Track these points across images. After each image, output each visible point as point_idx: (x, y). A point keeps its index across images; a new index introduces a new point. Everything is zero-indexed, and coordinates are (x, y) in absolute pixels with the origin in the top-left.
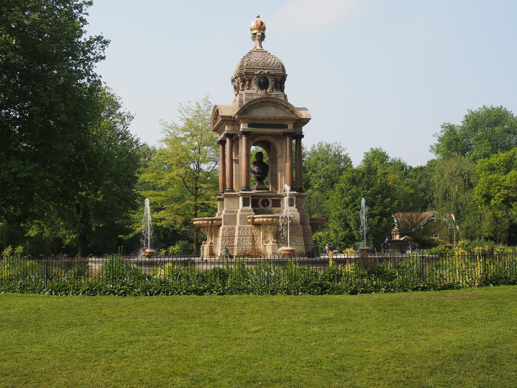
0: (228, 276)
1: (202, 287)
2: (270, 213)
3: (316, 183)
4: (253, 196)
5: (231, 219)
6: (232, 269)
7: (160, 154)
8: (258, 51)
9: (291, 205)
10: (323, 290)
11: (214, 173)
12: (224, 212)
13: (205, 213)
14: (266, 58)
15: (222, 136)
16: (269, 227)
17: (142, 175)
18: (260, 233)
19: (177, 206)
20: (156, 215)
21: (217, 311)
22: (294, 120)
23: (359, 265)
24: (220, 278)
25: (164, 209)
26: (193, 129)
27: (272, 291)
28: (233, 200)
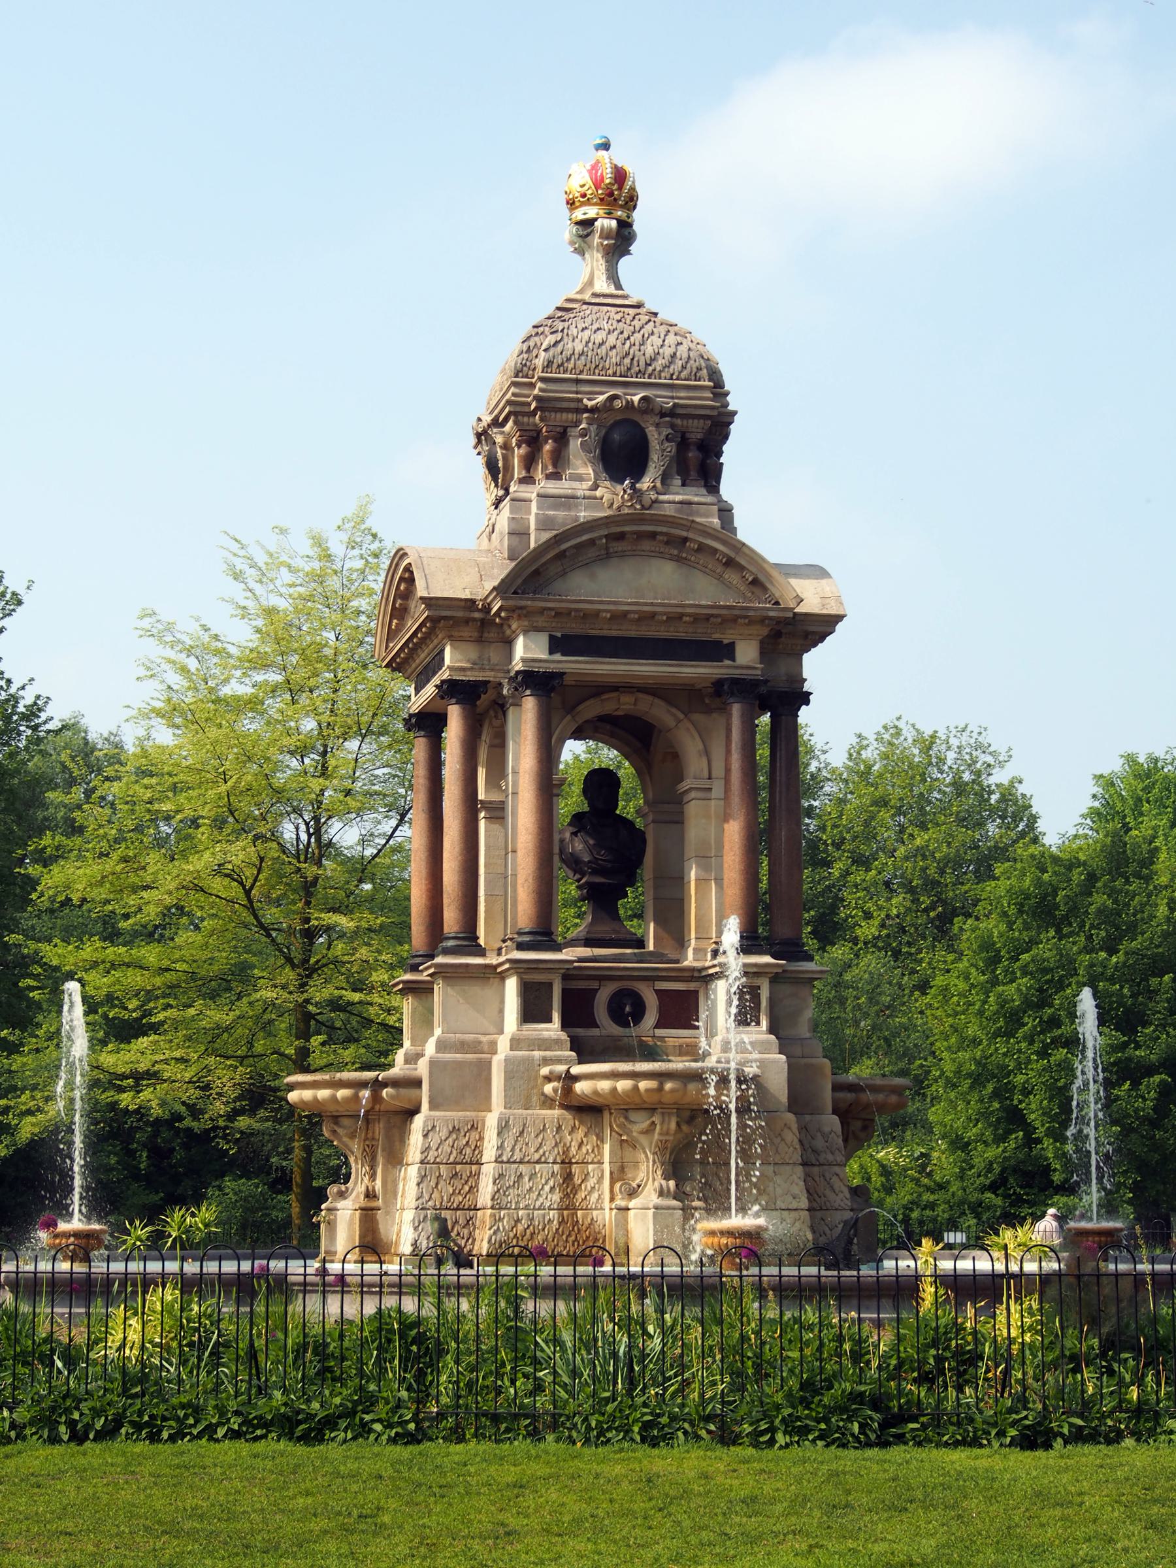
0: (441, 1352)
1: (316, 1405)
2: (650, 1054)
3: (868, 916)
4: (569, 974)
5: (466, 1081)
6: (460, 1318)
7: (143, 773)
8: (598, 301)
9: (745, 1018)
10: (888, 1422)
11: (393, 865)
12: (430, 1048)
13: (348, 1053)
14: (638, 336)
15: (430, 690)
16: (641, 1122)
17: (55, 869)
18: (598, 1148)
19: (217, 1015)
20: (117, 1059)
21: (386, 1519)
22: (763, 620)
23: (1061, 1307)
24: (404, 1360)
25: (155, 1028)
26: (294, 659)
27: (646, 1426)
28: (476, 990)
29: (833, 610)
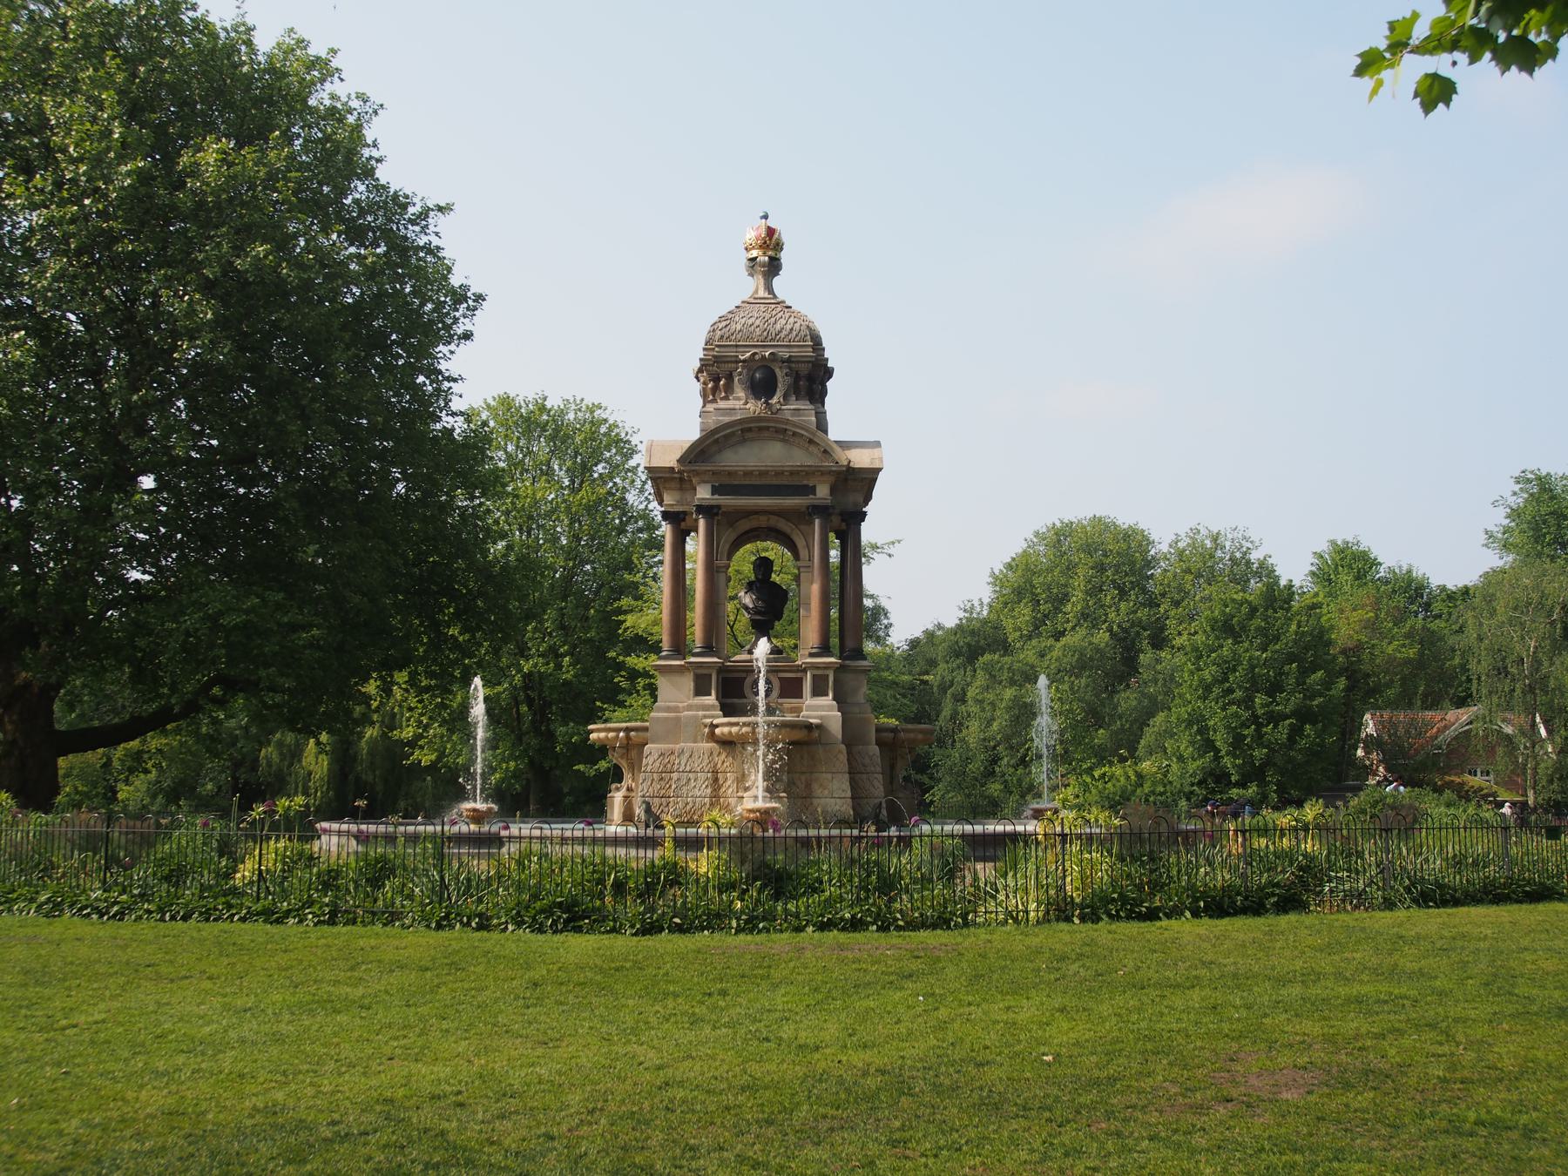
29: (877, 466)
